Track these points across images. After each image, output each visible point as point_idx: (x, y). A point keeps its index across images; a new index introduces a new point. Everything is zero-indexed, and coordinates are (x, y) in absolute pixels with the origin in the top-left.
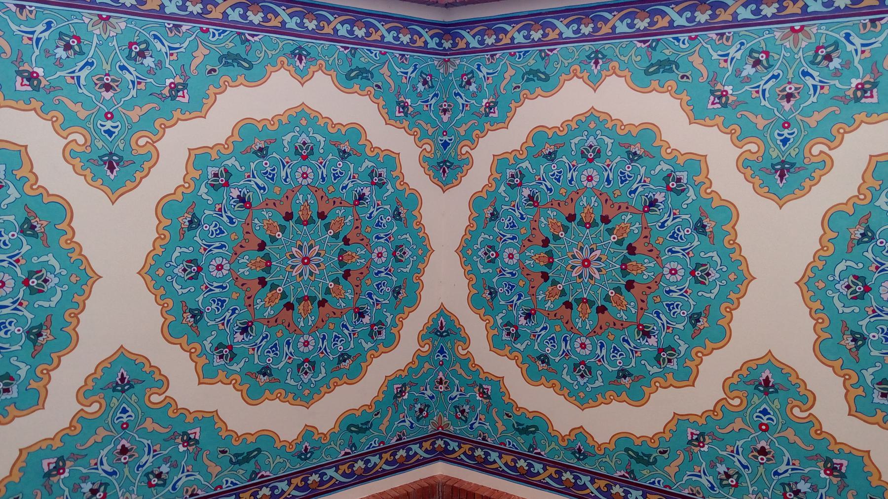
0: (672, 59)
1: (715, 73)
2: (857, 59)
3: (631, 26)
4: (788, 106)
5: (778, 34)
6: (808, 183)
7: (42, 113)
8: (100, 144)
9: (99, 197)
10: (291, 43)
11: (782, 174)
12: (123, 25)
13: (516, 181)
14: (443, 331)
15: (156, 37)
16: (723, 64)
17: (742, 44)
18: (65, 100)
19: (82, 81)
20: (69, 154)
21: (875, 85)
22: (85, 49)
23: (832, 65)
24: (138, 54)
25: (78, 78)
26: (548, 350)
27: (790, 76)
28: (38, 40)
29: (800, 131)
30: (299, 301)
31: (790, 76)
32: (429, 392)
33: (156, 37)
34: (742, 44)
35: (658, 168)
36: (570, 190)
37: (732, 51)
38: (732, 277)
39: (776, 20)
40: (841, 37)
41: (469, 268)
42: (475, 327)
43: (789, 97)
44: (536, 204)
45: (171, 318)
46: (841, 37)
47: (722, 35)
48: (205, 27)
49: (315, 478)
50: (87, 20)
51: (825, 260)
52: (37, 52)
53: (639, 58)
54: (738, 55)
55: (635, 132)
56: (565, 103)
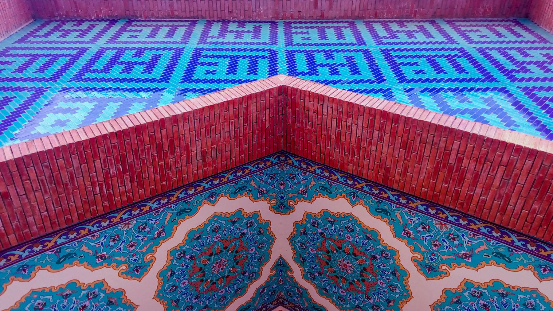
0: (388, 210)
1: (406, 224)
2: (465, 245)
3: (371, 190)
4: (435, 248)
5: (434, 222)
6: (439, 277)
7: (108, 266)
8: (132, 266)
9: (135, 282)
10: (207, 193)
11: (430, 270)
12: (135, 222)
13: (316, 225)
14: (281, 265)
15: (149, 219)
16: (409, 222)
17: (419, 219)
18: (116, 258)
19: (122, 249)
20: (121, 275)
21: (470, 256)
22: (120, 238)
23: (455, 242)
24: (142, 229)
25: (120, 248)
26: (333, 227)
27: (437, 238)
28: (102, 243)
29: (438, 258)
30: (218, 280)
31: (437, 238)
32: (275, 286)
33: (149, 219)
34: (419, 219)
35: (378, 247)
36: (340, 238)
37: (414, 219)
38: (405, 294)
39: (433, 216)
40: (460, 234)
41: (293, 247)
42: (297, 272)
43: (436, 245)
44: (324, 236)
45: (166, 307)
46: (460, 234)
47: (410, 212)
48: (169, 206)
49: (216, 182)
50: (120, 228)
51: (442, 303)
52: (102, 247)
53: (373, 204)
54: (417, 222)
55: (369, 230)
56: (340, 206)
